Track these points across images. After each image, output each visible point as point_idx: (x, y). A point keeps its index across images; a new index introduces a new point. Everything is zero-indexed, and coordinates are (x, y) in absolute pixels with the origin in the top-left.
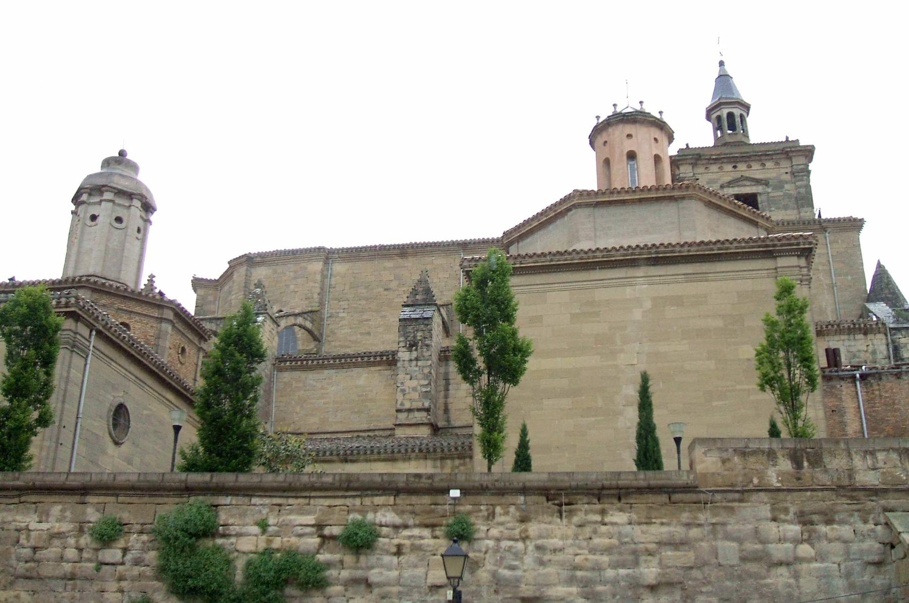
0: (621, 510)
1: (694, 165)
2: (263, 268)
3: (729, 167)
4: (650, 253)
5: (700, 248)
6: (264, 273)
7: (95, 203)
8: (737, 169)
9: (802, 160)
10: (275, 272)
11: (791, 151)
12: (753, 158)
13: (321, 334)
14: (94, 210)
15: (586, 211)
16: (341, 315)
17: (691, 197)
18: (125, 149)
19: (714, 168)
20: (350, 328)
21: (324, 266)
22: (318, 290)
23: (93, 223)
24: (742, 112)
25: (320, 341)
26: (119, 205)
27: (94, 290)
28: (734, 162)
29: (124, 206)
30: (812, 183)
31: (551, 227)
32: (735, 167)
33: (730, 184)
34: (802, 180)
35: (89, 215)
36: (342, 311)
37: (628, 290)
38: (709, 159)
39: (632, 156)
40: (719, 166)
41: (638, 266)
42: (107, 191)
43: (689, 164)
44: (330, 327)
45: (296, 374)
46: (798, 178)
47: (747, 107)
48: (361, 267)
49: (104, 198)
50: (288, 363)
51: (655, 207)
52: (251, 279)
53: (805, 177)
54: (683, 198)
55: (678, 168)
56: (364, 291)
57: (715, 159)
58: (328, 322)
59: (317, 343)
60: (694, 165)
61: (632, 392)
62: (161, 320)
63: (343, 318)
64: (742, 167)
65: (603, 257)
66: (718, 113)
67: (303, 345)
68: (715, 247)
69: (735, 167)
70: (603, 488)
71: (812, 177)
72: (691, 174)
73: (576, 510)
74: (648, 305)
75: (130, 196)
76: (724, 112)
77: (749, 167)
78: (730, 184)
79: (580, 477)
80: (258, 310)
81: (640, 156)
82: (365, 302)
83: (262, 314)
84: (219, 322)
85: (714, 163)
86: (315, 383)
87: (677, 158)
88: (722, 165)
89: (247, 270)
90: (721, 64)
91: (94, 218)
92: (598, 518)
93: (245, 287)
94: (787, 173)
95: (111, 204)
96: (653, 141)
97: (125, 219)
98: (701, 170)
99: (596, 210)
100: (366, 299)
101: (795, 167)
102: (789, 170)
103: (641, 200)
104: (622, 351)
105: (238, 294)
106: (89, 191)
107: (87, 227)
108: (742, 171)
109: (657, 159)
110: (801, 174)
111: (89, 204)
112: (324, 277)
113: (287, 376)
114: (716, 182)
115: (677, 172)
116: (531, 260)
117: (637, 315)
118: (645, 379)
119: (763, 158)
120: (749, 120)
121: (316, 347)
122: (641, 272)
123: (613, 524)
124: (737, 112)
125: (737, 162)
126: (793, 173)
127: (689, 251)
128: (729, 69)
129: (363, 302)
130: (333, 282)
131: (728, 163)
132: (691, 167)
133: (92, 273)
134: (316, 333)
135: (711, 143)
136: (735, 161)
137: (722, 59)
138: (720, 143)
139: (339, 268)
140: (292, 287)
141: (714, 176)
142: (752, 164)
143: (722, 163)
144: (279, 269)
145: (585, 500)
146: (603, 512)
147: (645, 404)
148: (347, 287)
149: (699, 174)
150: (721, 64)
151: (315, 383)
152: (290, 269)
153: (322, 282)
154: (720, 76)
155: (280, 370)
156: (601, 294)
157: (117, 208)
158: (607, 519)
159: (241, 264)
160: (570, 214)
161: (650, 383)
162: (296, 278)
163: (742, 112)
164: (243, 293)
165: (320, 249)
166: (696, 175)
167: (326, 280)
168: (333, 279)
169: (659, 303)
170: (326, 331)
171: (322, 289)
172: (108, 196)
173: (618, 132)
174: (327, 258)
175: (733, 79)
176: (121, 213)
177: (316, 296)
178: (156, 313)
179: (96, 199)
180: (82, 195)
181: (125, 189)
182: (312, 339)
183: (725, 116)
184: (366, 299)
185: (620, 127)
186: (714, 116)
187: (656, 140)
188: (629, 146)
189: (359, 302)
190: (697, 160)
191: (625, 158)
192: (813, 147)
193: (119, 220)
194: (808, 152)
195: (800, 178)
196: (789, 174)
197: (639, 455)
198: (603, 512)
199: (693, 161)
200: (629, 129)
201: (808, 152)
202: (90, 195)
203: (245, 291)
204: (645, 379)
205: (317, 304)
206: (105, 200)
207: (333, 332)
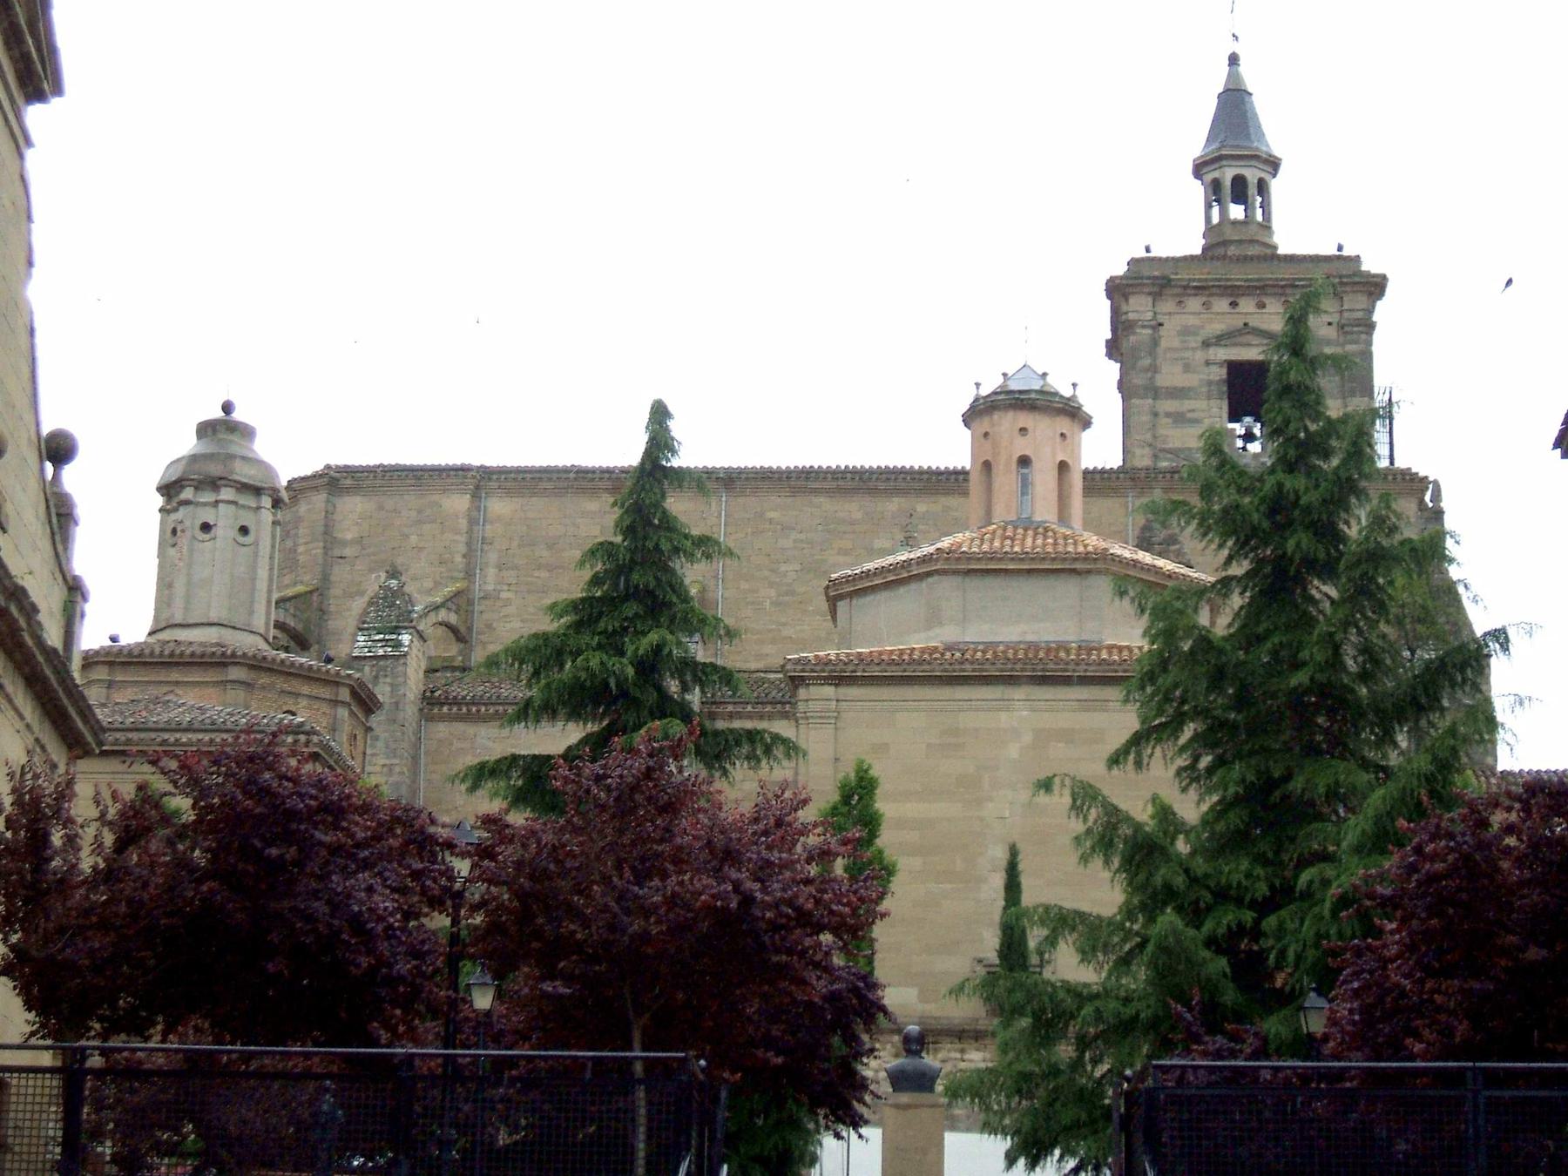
0: (977, 1050)
1: (1157, 296)
2: (358, 499)
3: (1221, 305)
4: (1034, 670)
5: (1101, 668)
6: (359, 508)
7: (205, 504)
8: (1238, 310)
9: (1361, 301)
10: (381, 508)
11: (1342, 283)
12: (1270, 290)
13: (470, 629)
14: (208, 516)
15: (957, 580)
16: (504, 595)
17: (1099, 572)
18: (231, 399)
19: (1194, 304)
20: (522, 621)
21: (472, 502)
22: (462, 548)
23: (207, 537)
24: (1263, 175)
25: (466, 642)
26: (243, 507)
27: (252, 667)
28: (1231, 295)
29: (249, 508)
30: (1375, 349)
31: (902, 590)
32: (1234, 304)
33: (1221, 340)
34: (1356, 342)
35: (198, 523)
36: (506, 587)
37: (1003, 716)
38: (1185, 288)
39: (1024, 461)
40: (1204, 299)
41: (1020, 685)
42: (226, 486)
43: (1150, 294)
44: (485, 616)
45: (460, 727)
46: (1349, 337)
47: (1274, 164)
48: (537, 507)
49: (222, 497)
50: (445, 709)
51: (1052, 581)
52: (335, 517)
53: (1363, 336)
54: (1089, 572)
55: (1127, 300)
56: (545, 553)
57: (1196, 288)
58: (481, 608)
59: (462, 646)
60: (1157, 296)
61: (1000, 855)
62: (335, 703)
63: (508, 602)
64: (1247, 305)
65: (974, 670)
66: (1216, 174)
67: (436, 648)
68: (1120, 668)
69: (1234, 304)
70: (964, 1031)
71: (1377, 336)
72: (1149, 315)
73: (941, 1049)
74: (1028, 738)
75: (257, 491)
76: (1228, 174)
77: (1262, 306)
78: (1221, 340)
79: (945, 1022)
80: (398, 621)
81: (1037, 464)
82: (548, 574)
83: (405, 628)
84: (288, 604)
85: (1196, 295)
86: (491, 744)
87: (1124, 282)
88: (1212, 299)
89: (328, 501)
90: (1234, 60)
91: (206, 527)
92: (958, 1055)
93: (325, 533)
94: (1330, 324)
95: (233, 507)
96: (1058, 439)
97: (252, 528)
98: (1167, 305)
99: (967, 580)
100: (551, 568)
101: (1346, 315)
102: (1335, 318)
103: (1029, 571)
104: (991, 799)
105: (311, 546)
106: (195, 483)
107: (196, 543)
108: (1246, 314)
109: (1063, 467)
110: (1355, 329)
111: (197, 504)
112: (472, 522)
113: (442, 730)
114: (1195, 334)
115: (1124, 308)
116: (877, 668)
117: (1013, 751)
118: (1014, 852)
119: (1288, 291)
120: (1276, 186)
121: (460, 653)
122: (1019, 693)
123: (971, 1061)
124: (1252, 175)
125: (1238, 296)
126: (1341, 327)
127: (1086, 671)
128: (1251, 79)
129: (544, 574)
130: (489, 534)
131: (1221, 295)
132: (1150, 299)
133: (216, 621)
134: (463, 629)
135: (1195, 246)
136: (1233, 292)
137: (1237, 48)
138: (1218, 241)
139: (499, 506)
140: (414, 539)
141: (1192, 321)
142: (1267, 300)
143: (1211, 295)
144: (390, 503)
145: (948, 1040)
146: (962, 1051)
147: (1013, 887)
148: (515, 544)
149: (1165, 314)
150: (1234, 60)
151: (491, 744)
152: (409, 503)
153: (470, 532)
154: (1227, 91)
155: (430, 719)
156: (968, 720)
157: (241, 512)
158: (966, 1057)
159: (316, 488)
160: (930, 580)
161: (1020, 857)
162: (420, 522)
163: (1263, 175)
164: (321, 544)
165: (464, 469)
166: (1159, 317)
167: (475, 528)
168: (488, 527)
169: (1043, 737)
170: (478, 625)
171: (469, 544)
172: (227, 494)
173: (1007, 422)
174: (477, 487)
175: (1254, 98)
176: (247, 519)
177: (458, 559)
178: (325, 692)
179: (207, 497)
180: (183, 487)
181: (252, 482)
182: (454, 639)
183: (1227, 183)
184: (551, 568)
185: (1011, 414)
186: (1209, 177)
187: (1062, 435)
188: (1022, 447)
189: (536, 574)
190: (1163, 287)
191: (1014, 465)
192: (1384, 278)
193: (244, 530)
194: (1375, 286)
195: (1355, 336)
196: (1333, 328)
197: (1002, 945)
198: (962, 1051)
199: (1156, 289)
200: (1025, 419)
201: (1375, 286)
202: (196, 488)
203: (325, 541)
204: (1014, 852)
205: (462, 575)
206: (223, 501)
207: (489, 626)
